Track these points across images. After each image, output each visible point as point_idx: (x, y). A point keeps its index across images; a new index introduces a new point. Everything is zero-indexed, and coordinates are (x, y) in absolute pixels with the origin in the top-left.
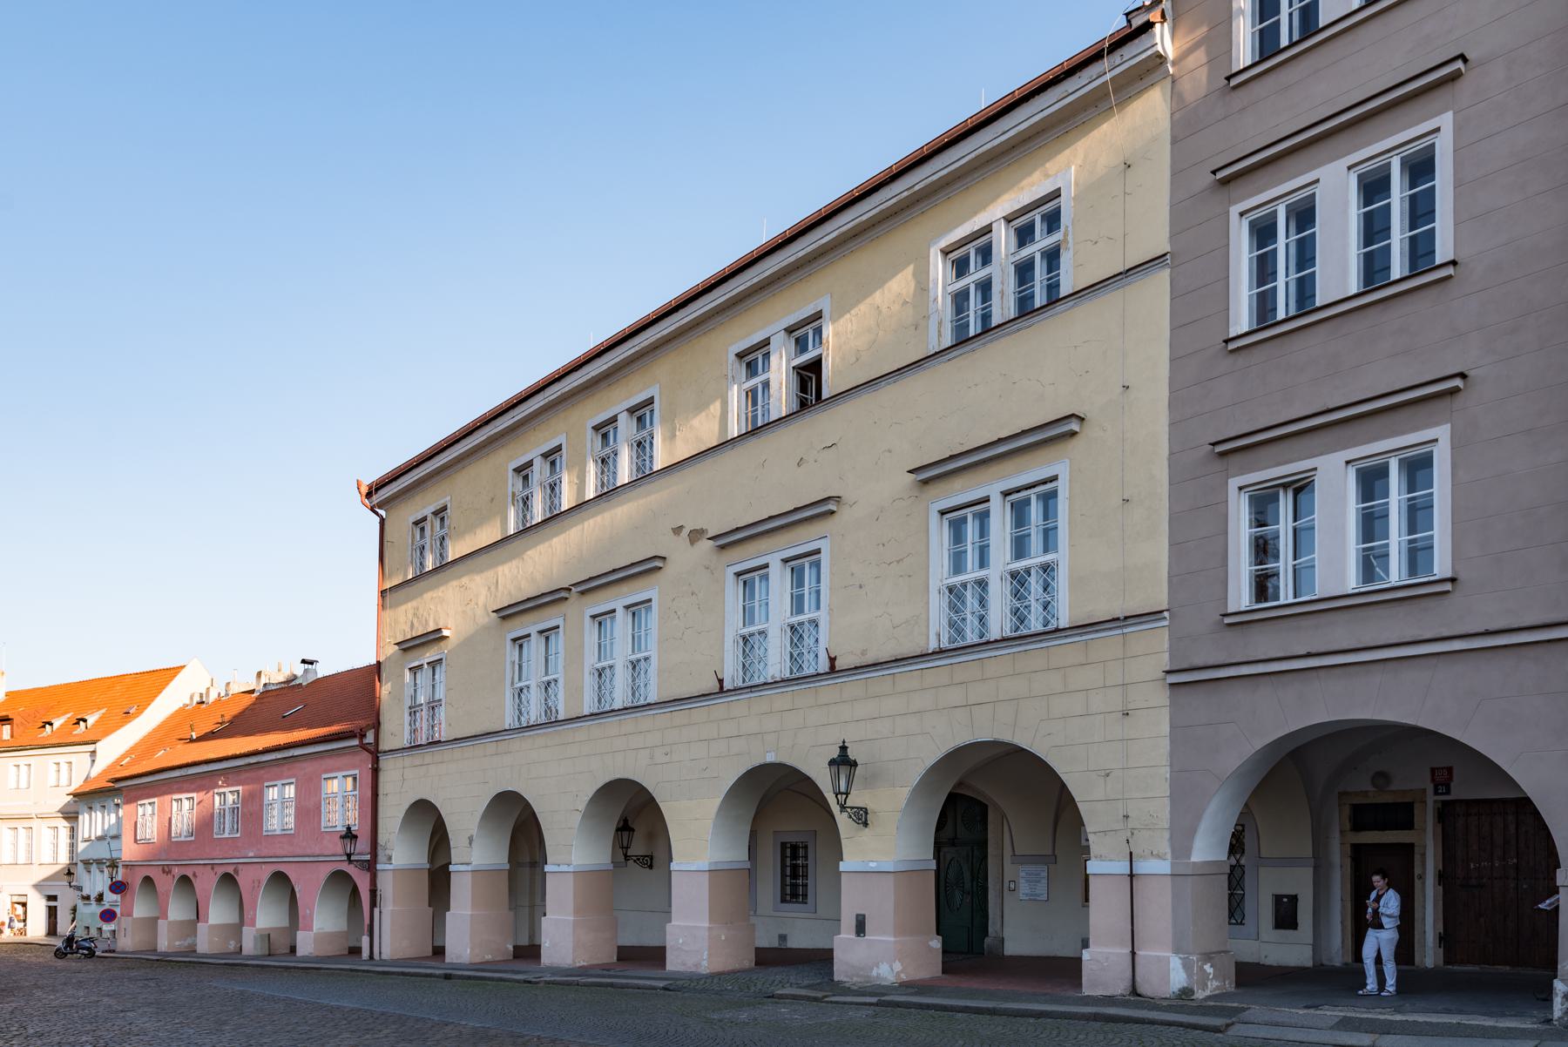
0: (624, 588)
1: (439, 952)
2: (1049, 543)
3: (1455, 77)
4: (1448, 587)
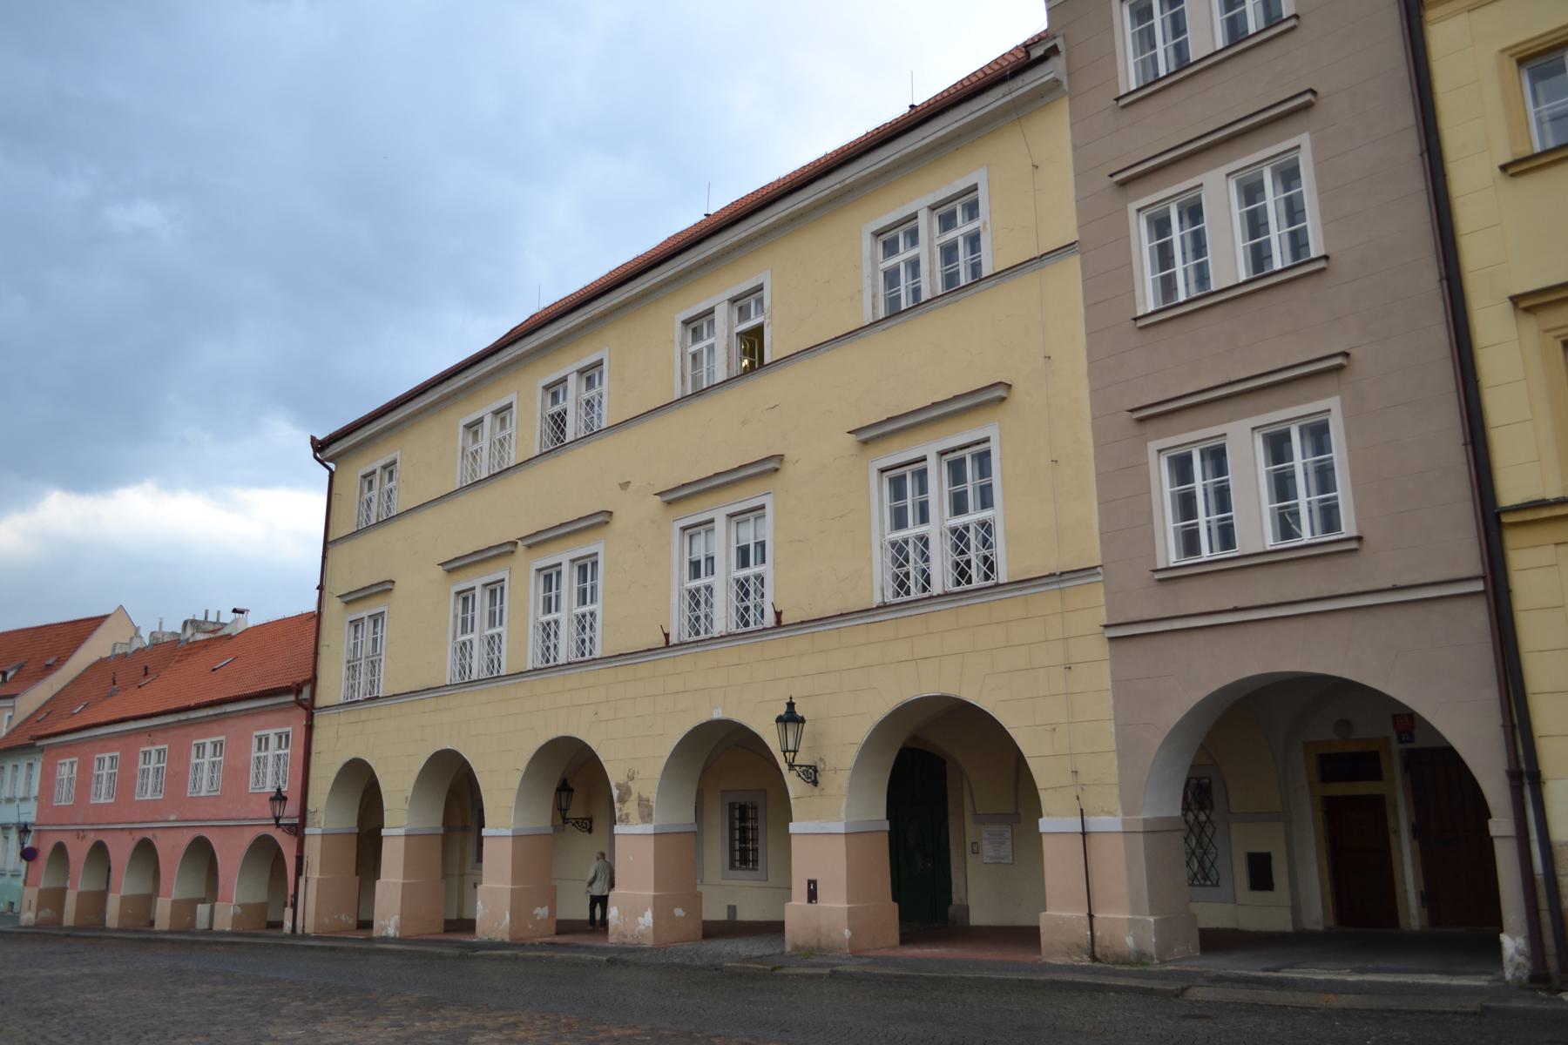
0: (571, 542)
1: (366, 925)
2: (986, 501)
3: (1307, 106)
4: (1353, 545)
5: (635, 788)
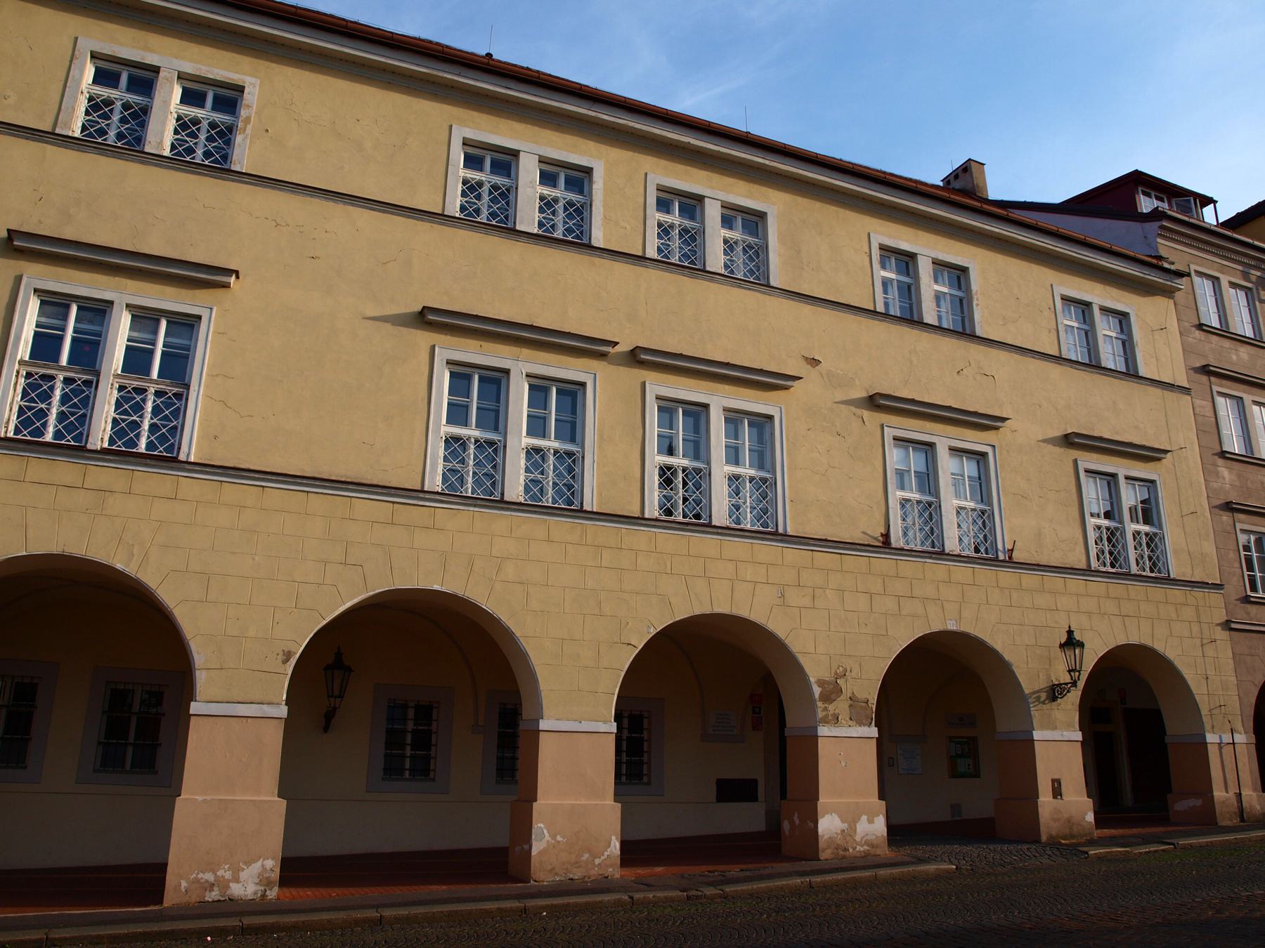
5: (848, 687)
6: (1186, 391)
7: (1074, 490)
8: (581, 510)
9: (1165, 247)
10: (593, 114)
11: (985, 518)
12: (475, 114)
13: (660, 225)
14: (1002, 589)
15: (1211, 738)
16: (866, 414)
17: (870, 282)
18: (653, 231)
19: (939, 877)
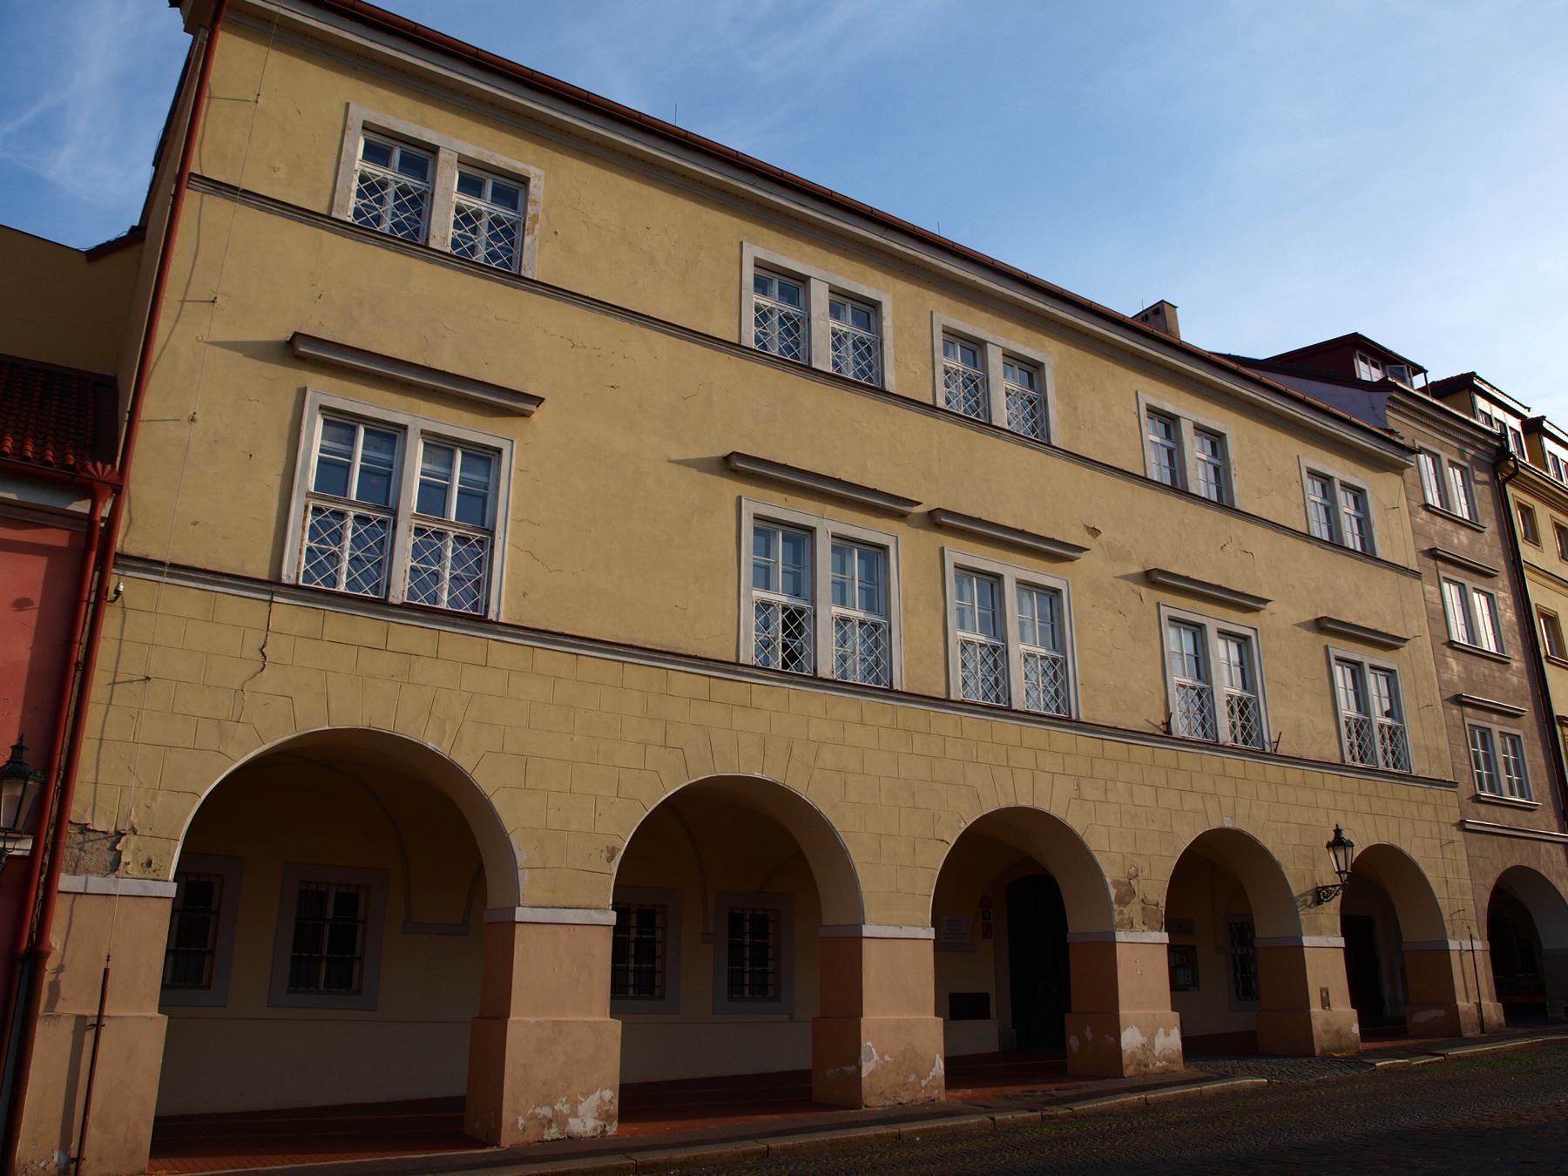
5: (1140, 887)
6: (1417, 575)
7: (1326, 679)
8: (891, 690)
9: (1394, 420)
10: (884, 241)
11: (1057, 667)
12: (764, 230)
13: (758, 309)
14: (1269, 784)
15: (1453, 945)
16: (1144, 590)
17: (740, 313)
18: (749, 316)
19: (1256, 1091)
